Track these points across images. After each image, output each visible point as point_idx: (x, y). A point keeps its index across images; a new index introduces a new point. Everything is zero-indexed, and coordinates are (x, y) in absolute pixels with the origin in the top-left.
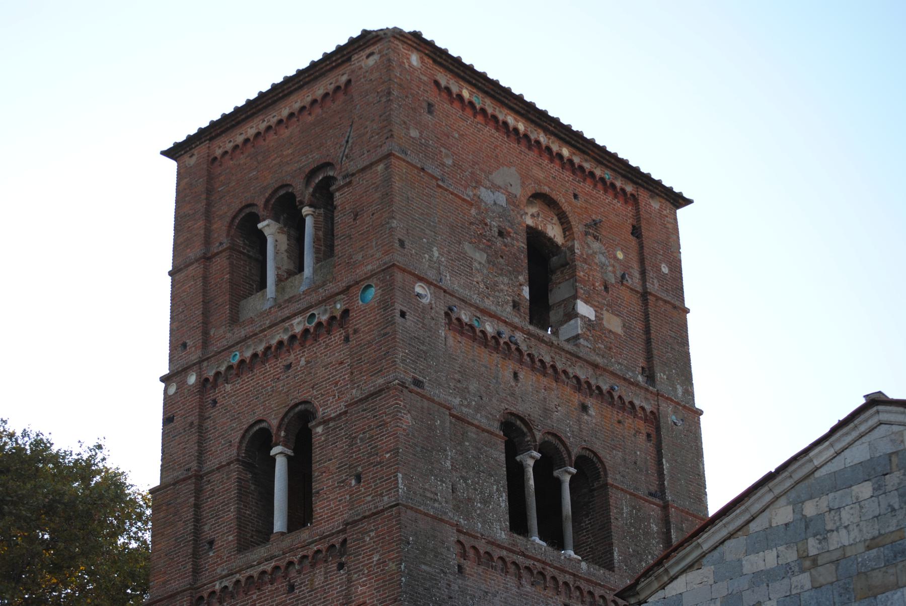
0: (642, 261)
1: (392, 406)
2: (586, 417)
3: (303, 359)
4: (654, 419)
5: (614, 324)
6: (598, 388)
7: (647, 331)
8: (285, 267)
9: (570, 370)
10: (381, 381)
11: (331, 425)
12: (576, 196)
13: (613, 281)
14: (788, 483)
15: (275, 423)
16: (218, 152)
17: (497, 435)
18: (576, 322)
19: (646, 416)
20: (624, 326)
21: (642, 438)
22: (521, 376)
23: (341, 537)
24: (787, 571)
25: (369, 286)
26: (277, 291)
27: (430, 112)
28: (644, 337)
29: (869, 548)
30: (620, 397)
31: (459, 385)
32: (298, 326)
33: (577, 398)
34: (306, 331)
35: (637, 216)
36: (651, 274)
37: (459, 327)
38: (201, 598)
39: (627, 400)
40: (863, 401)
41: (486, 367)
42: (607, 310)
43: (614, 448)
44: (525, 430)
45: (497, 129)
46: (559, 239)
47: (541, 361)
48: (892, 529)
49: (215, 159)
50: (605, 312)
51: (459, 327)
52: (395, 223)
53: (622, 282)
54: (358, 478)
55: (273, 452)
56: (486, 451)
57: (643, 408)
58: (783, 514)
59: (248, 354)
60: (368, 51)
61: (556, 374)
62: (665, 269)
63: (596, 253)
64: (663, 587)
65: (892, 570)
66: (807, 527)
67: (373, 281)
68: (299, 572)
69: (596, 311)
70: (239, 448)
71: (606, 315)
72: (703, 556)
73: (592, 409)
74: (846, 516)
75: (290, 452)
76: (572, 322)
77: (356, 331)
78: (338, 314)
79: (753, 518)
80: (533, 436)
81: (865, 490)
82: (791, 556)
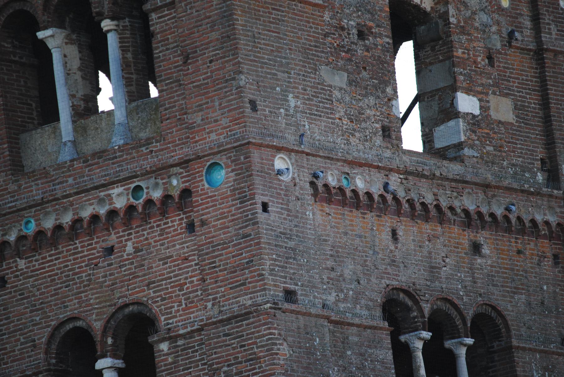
1: (264, 336)
2: (479, 261)
3: (129, 244)
6: (492, 215)
7: (545, 104)
8: (80, 94)
11: (180, 343)
13: (499, 46)
15: (98, 326)
17: (381, 329)
18: (458, 125)
19: (551, 232)
20: (516, 108)
21: (548, 263)
22: (400, 233)
25: (215, 164)
26: (75, 130)
28: (541, 113)
30: (519, 218)
31: (333, 275)
33: (465, 238)
34: (131, 208)
37: (327, 195)
39: (526, 218)
41: (360, 237)
42: (494, 93)
43: (516, 291)
44: (410, 303)
47: (423, 204)
50: (491, 97)
51: (327, 195)
52: (243, 80)
53: (510, 43)
56: (370, 356)
57: (547, 223)
63: (474, 13)
67: (222, 160)
69: (480, 100)
70: (47, 352)
71: (493, 100)
73: (485, 247)
75: (119, 363)
76: (452, 123)
77: (203, 223)
78: (176, 193)
80: (421, 310)
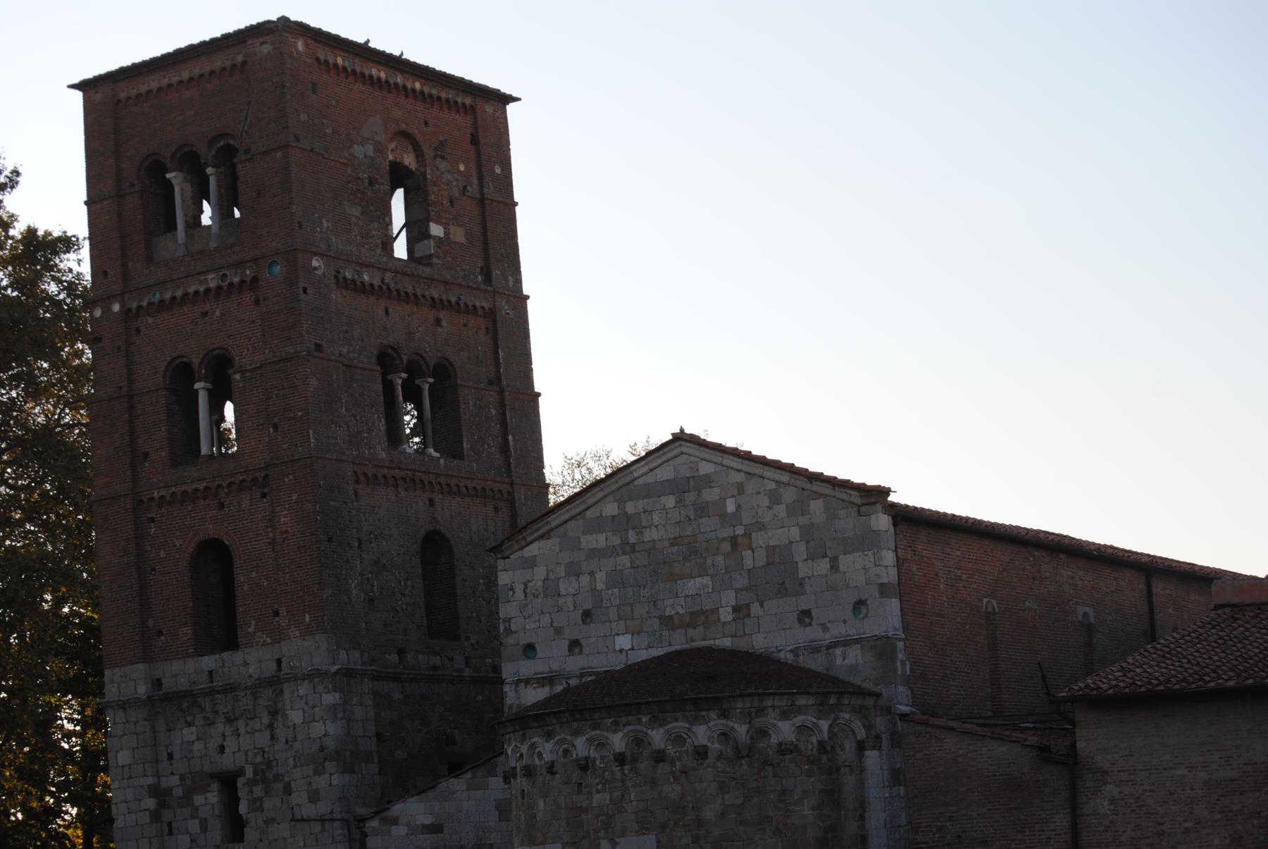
0: (479, 167)
4: (492, 315)
5: (459, 235)
9: (427, 293)
10: (291, 350)
12: (426, 124)
14: (615, 487)
15: (196, 362)
16: (123, 96)
21: (482, 332)
23: (263, 473)
24: (610, 552)
27: (314, 91)
29: (672, 545)
32: (212, 281)
34: (219, 288)
35: (475, 126)
36: (487, 179)
38: (142, 501)
40: (670, 437)
45: (364, 84)
46: (413, 166)
48: (689, 533)
49: (119, 101)
54: (276, 427)
55: (197, 386)
58: (610, 509)
59: (168, 296)
60: (261, 40)
61: (416, 300)
62: (498, 170)
64: (522, 549)
65: (688, 564)
66: (628, 521)
68: (228, 494)
71: (452, 228)
72: (552, 530)
74: (656, 517)
75: (209, 386)
77: (265, 299)
79: (589, 508)
80: (401, 360)
81: (670, 501)
82: (616, 541)
